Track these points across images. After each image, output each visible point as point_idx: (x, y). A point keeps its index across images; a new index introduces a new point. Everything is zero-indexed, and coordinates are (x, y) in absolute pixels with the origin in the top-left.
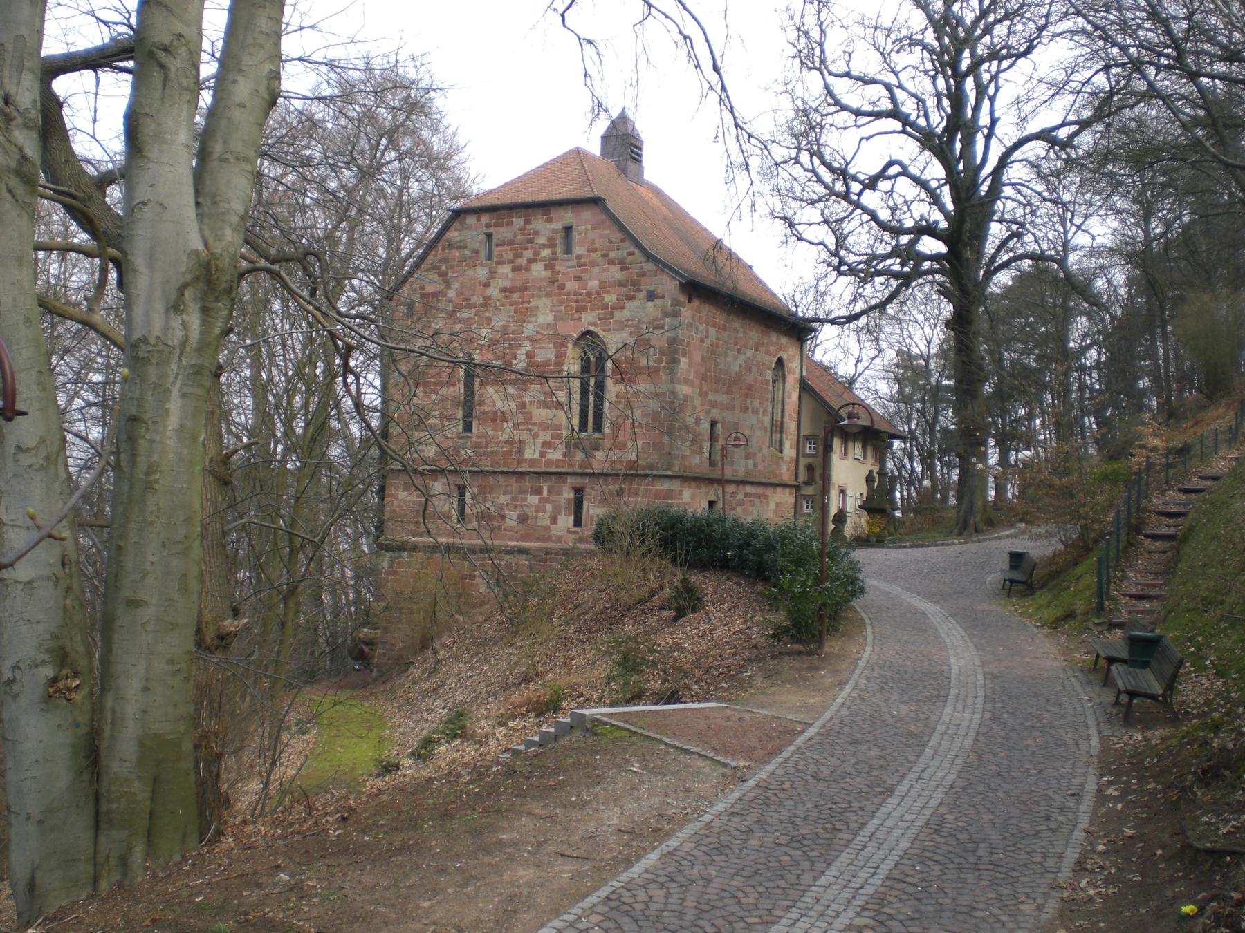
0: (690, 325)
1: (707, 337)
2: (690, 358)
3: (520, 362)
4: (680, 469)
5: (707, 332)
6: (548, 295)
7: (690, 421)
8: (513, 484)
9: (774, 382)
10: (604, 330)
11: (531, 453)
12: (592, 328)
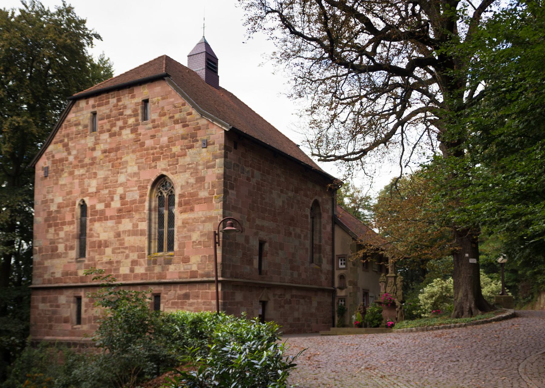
1: (253, 177)
3: (116, 204)
5: (253, 173)
9: (313, 218)
10: (172, 174)
11: (124, 270)
12: (164, 173)
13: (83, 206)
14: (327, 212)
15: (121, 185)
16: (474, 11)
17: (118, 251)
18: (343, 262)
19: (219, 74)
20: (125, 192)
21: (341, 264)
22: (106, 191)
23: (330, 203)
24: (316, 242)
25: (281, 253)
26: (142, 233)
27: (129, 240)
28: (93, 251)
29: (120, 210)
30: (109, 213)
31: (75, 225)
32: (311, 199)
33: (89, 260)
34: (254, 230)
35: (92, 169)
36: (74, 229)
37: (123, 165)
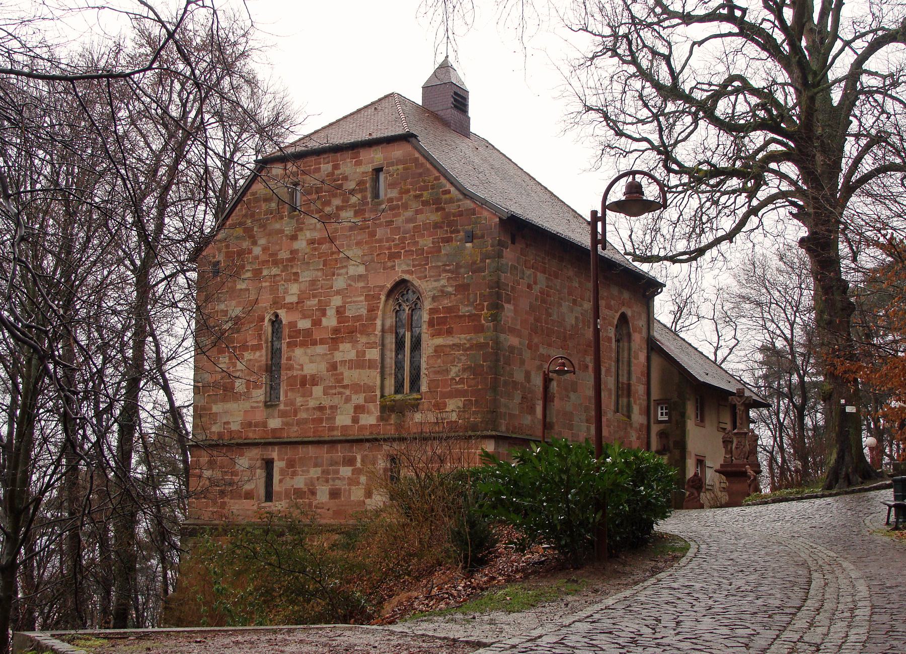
0: (514, 268)
1: (535, 283)
2: (516, 305)
3: (330, 321)
4: (508, 430)
5: (535, 276)
6: (358, 244)
7: (519, 376)
8: (323, 453)
9: (618, 341)
10: (420, 278)
11: (343, 419)
12: (406, 277)
13: (276, 322)
14: (640, 333)
15: (338, 293)
16: (856, 57)
17: (334, 391)
18: (664, 411)
19: (470, 114)
20: (345, 303)
21: (662, 414)
22: (315, 302)
23: (644, 317)
24: (624, 379)
25: (572, 396)
26: (371, 364)
27: (350, 376)
28: (292, 390)
29: (336, 331)
30: (317, 336)
31: (264, 352)
32: (616, 312)
33: (286, 405)
34: (537, 363)
35: (292, 266)
36: (260, 357)
37: (341, 262)
